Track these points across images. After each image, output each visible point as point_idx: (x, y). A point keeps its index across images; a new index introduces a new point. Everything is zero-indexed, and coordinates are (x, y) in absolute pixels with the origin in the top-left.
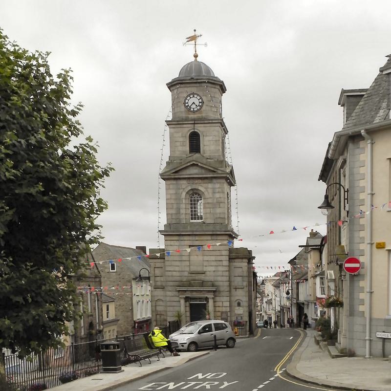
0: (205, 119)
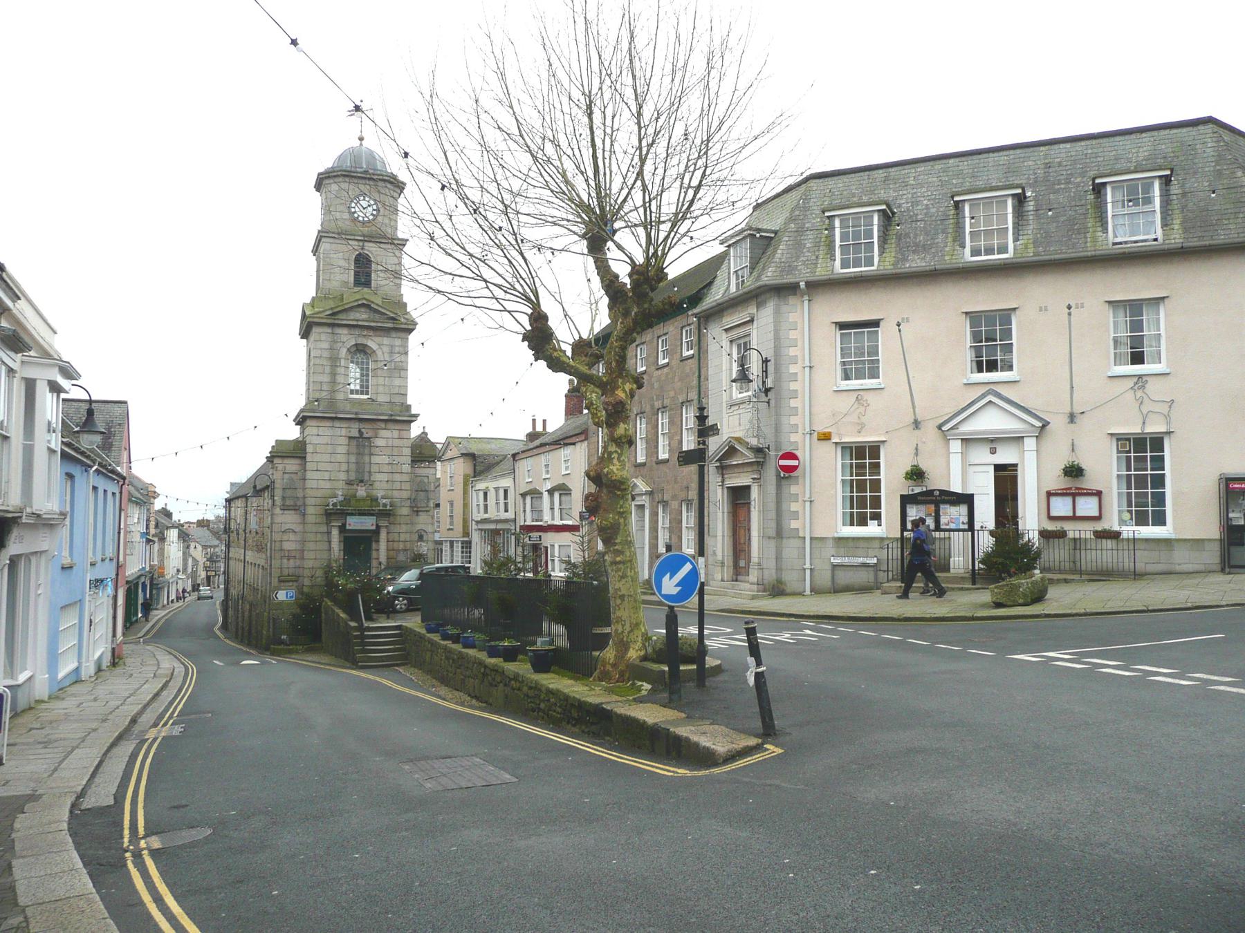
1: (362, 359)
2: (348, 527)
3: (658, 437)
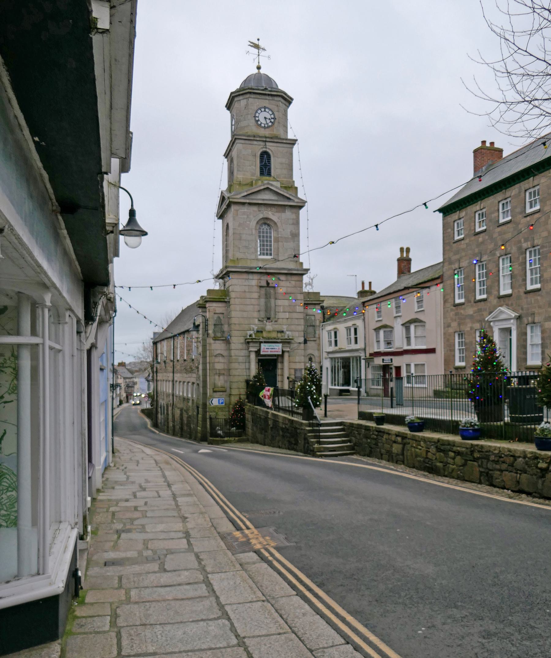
0: (277, 137)
1: (267, 229)
2: (262, 353)
3: (499, 278)
